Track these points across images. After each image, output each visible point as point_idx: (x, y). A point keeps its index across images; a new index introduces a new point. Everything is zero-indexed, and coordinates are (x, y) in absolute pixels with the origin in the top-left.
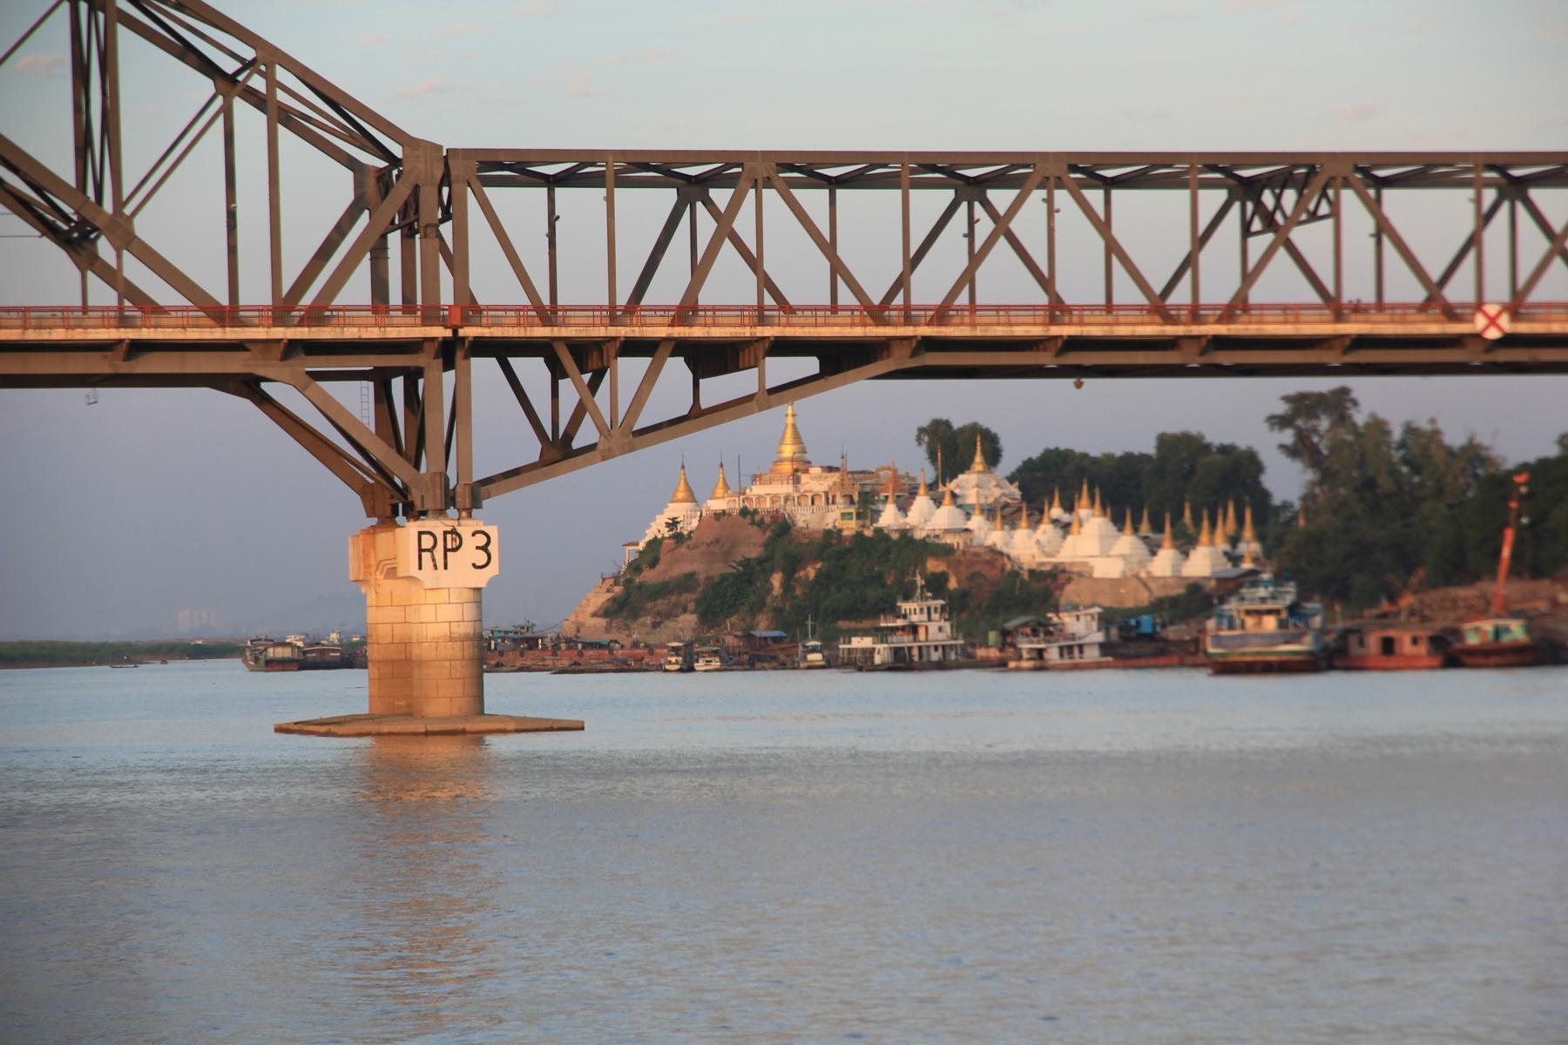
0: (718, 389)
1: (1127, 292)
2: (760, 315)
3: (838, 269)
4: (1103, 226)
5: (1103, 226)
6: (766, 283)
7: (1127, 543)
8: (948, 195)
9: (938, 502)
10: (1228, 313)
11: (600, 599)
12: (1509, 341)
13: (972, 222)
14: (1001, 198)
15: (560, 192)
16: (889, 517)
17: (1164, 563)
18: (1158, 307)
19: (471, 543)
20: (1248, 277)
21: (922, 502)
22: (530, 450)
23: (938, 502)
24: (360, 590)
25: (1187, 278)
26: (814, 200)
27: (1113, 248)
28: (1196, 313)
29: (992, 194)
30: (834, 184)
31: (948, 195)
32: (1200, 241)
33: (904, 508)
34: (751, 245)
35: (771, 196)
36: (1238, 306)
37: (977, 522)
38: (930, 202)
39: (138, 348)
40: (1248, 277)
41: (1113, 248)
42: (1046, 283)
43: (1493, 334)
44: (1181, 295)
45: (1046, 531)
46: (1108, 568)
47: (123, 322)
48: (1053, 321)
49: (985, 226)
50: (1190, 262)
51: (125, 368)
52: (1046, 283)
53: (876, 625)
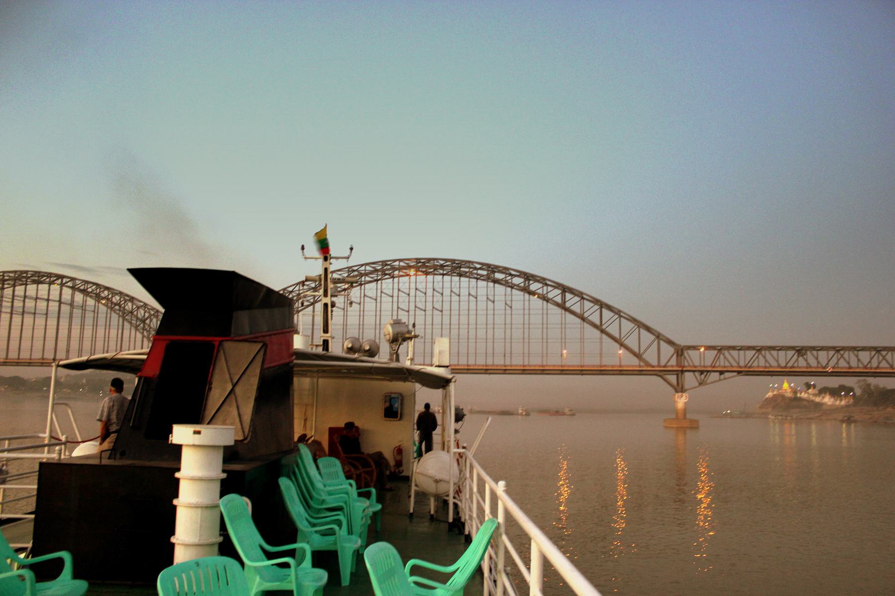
0: (722, 376)
1: (861, 365)
2: (807, 368)
3: (818, 362)
4: (857, 356)
5: (857, 356)
6: (808, 364)
7: (832, 400)
8: (834, 352)
9: (805, 393)
10: (876, 368)
11: (758, 406)
12: (832, 372)
13: (878, 357)
14: (884, 353)
15: (779, 352)
16: (798, 395)
17: (838, 403)
18: (865, 367)
19: (684, 396)
20: (879, 363)
21: (803, 394)
22: (697, 384)
23: (805, 393)
24: (675, 402)
25: (796, 362)
26: (815, 352)
27: (859, 360)
28: (871, 368)
29: (882, 352)
30: (818, 350)
31: (834, 352)
32: (872, 359)
33: (801, 394)
34: (847, 359)
35: (851, 352)
36: (877, 368)
37: (811, 396)
38: (832, 353)
39: (621, 370)
40: (879, 363)
41: (859, 360)
42: (849, 363)
43: (829, 371)
44: (869, 366)
45: (821, 398)
46: (830, 403)
47: (807, 368)
48: (871, 369)
49: (881, 358)
50: (870, 362)
51: (561, 373)
52: (849, 363)
53: (128, 402)
